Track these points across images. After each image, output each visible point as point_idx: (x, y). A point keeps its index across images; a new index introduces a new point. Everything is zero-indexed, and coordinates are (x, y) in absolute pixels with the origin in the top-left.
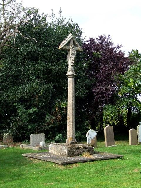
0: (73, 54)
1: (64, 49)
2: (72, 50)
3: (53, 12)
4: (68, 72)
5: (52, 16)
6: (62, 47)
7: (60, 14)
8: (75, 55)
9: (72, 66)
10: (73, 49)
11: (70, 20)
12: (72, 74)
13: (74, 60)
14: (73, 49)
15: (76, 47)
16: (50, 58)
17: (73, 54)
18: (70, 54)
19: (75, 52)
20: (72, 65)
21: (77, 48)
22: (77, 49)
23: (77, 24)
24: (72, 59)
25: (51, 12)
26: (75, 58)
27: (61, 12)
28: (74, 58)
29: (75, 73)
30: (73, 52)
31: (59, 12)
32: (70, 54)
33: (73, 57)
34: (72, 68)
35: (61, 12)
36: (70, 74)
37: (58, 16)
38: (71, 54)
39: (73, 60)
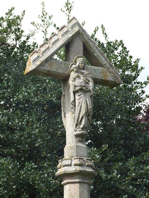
0: (83, 90)
1: (48, 74)
2: (78, 77)
3: (47, 10)
4: (65, 162)
5: (42, 23)
6: (38, 63)
7: (67, 12)
8: (88, 95)
9: (80, 137)
10: (83, 73)
11: (100, 30)
12: (78, 168)
13: (87, 114)
14: (83, 73)
15: (96, 68)
16: (31, 144)
17: (83, 90)
18: (71, 90)
19: (91, 84)
20: (78, 132)
21: (98, 72)
22: (100, 76)
23: (121, 42)
24: (77, 112)
25: (42, 10)
26: (90, 107)
27: (69, 7)
28: (84, 106)
29: (89, 166)
30: (79, 82)
31: (65, 9)
32: (71, 90)
33: (83, 103)
34: (80, 144)
35: (69, 7)
36: (72, 169)
37: (61, 20)
38: (75, 93)
39: (83, 112)
